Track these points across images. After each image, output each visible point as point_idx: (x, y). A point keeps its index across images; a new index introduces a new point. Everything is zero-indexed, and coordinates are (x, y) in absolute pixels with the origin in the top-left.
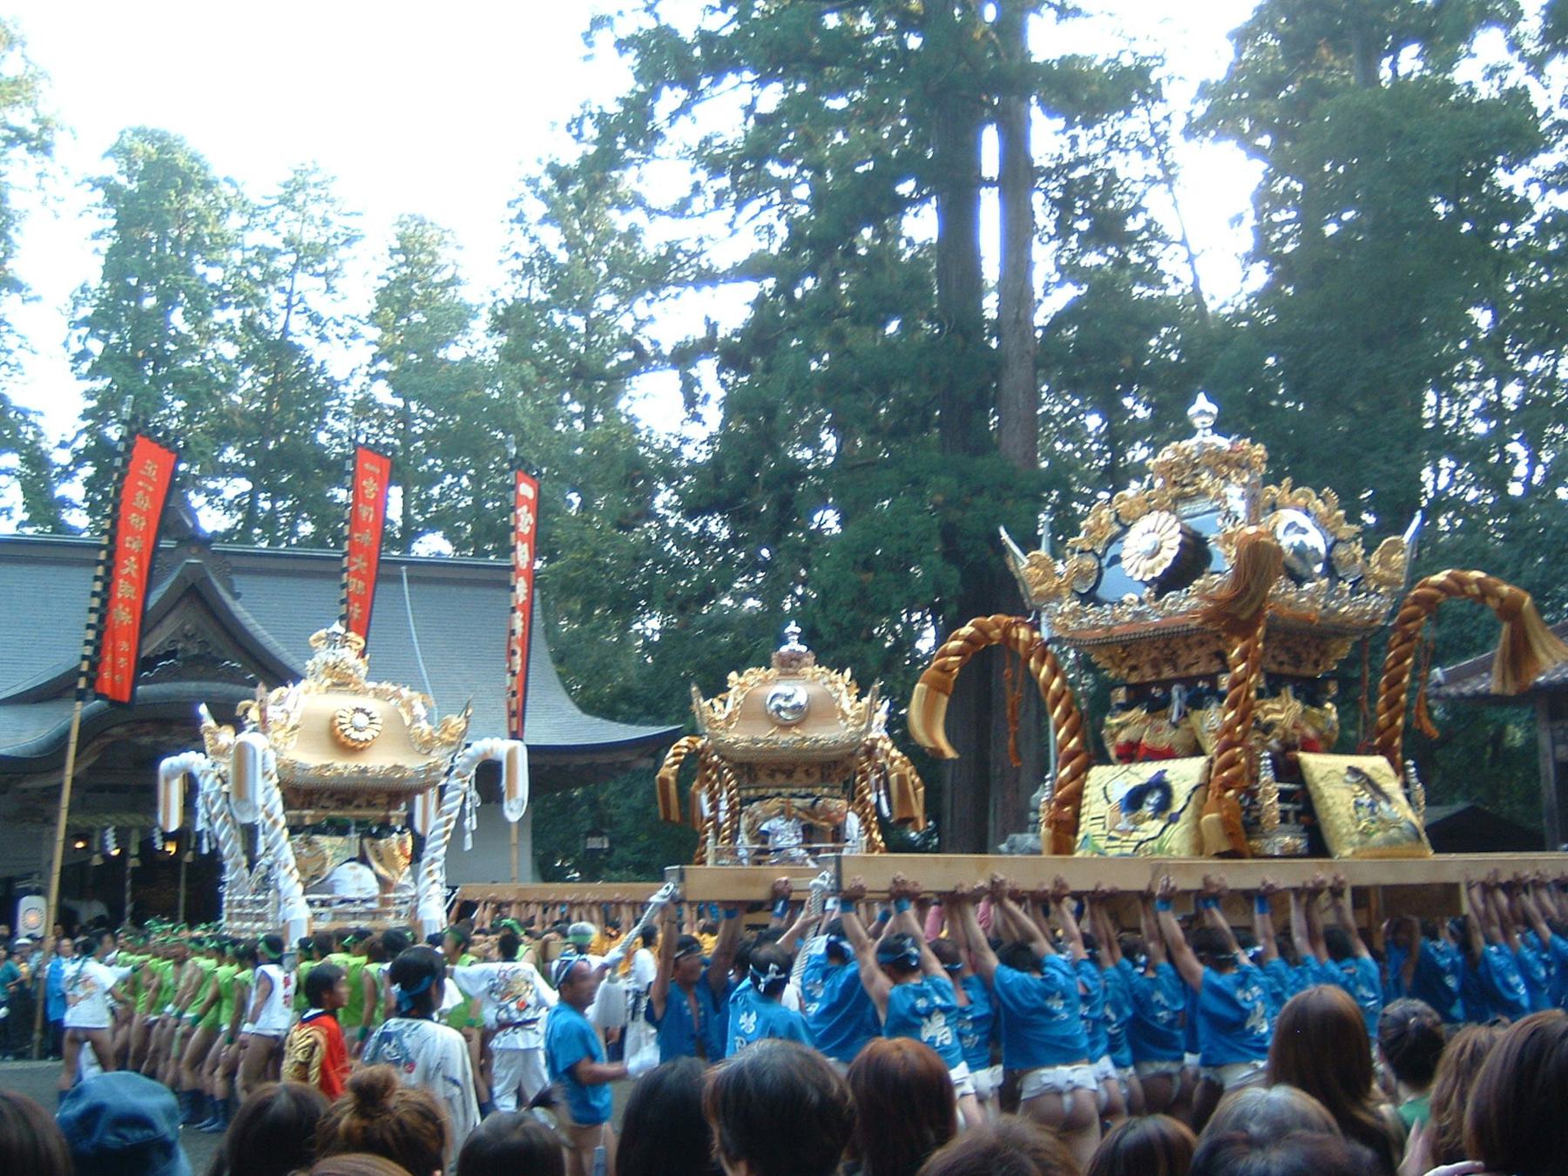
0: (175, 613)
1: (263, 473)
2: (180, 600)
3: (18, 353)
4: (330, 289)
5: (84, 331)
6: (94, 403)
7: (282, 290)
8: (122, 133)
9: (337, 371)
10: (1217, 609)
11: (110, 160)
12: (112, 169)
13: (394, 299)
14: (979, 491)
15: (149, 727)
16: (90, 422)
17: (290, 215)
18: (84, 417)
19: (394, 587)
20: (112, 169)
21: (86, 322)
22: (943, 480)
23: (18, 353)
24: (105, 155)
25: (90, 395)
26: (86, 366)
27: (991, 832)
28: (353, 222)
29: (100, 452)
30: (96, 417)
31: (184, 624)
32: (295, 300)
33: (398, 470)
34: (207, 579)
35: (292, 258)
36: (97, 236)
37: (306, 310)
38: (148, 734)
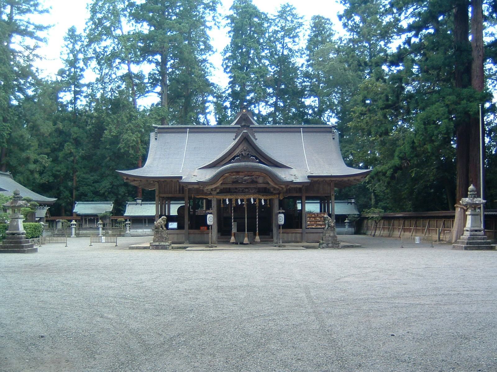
0: (242, 143)
1: (280, 94)
2: (243, 141)
3: (210, 69)
4: (294, 42)
5: (227, 61)
6: (232, 79)
7: (281, 43)
8: (234, 2)
9: (298, 64)
10: (394, 170)
11: (231, 10)
12: (231, 12)
13: (313, 43)
14: (463, 99)
15: (234, 174)
16: (231, 85)
17: (282, 21)
18: (229, 84)
19: (299, 134)
20: (231, 12)
21: (227, 59)
22: (450, 97)
23: (210, 69)
24: (230, 9)
25: (230, 77)
26: (228, 70)
27: (458, 195)
28: (300, 21)
29: (235, 94)
30: (232, 84)
31: (243, 148)
32: (285, 45)
33: (314, 92)
34: (248, 135)
35: (283, 33)
36: (229, 32)
37: (288, 48)
38: (234, 175)
